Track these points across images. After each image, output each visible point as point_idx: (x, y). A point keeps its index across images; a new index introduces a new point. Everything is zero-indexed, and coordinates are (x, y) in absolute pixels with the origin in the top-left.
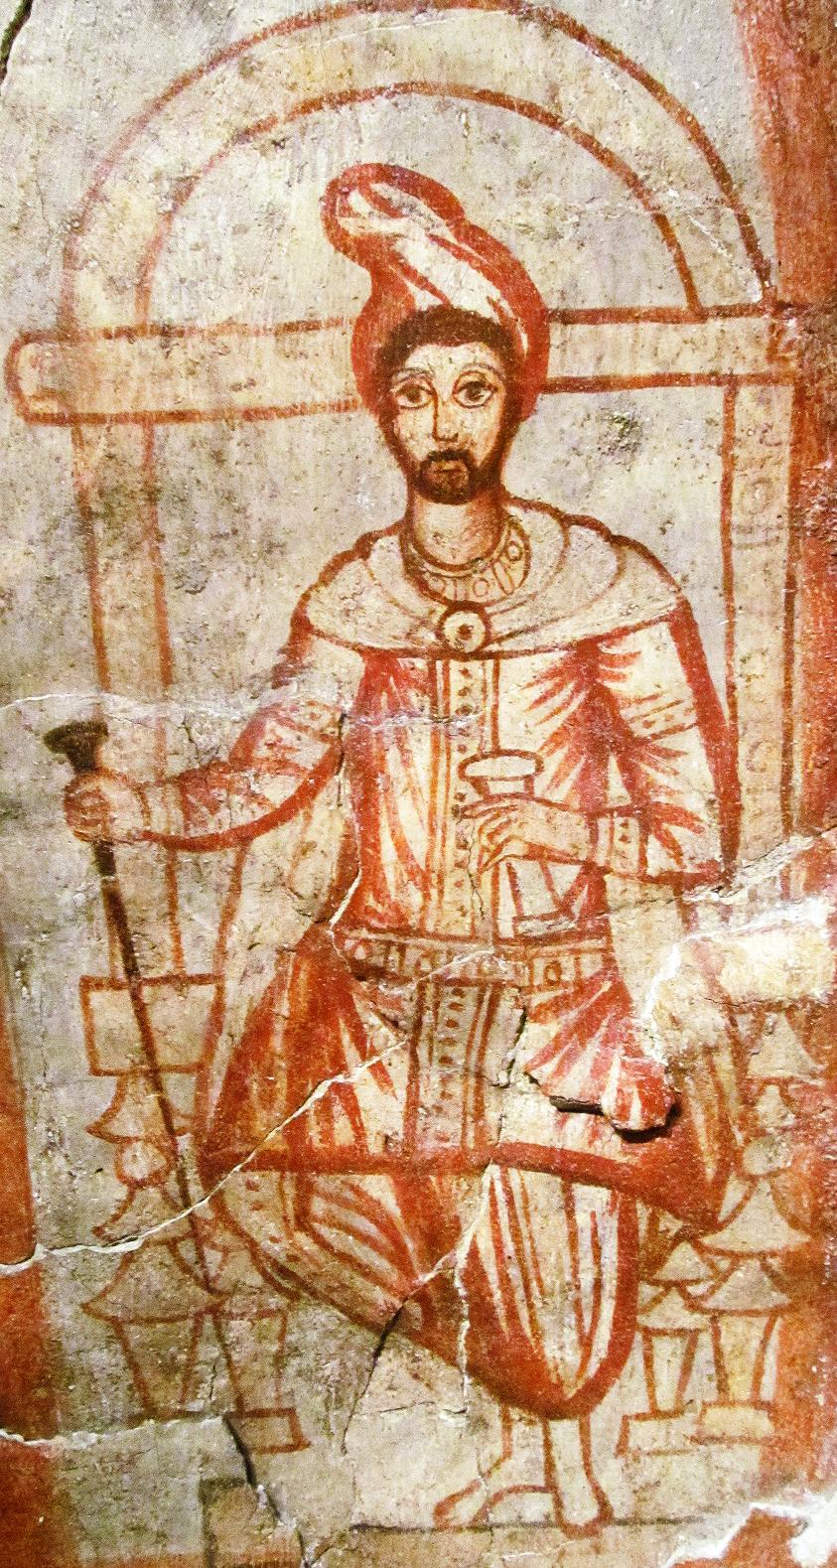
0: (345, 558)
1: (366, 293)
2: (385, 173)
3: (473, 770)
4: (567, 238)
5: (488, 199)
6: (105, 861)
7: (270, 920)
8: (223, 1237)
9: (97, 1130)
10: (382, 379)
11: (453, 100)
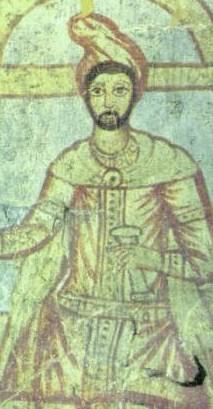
3: (115, 233)
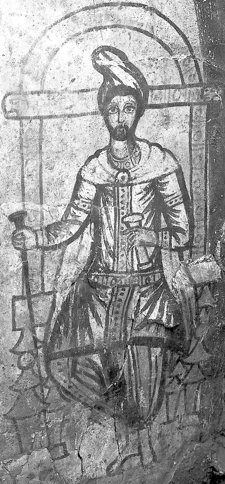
0: (90, 158)
1: (102, 81)
2: (109, 48)
3: (127, 219)
4: (154, 66)
5: (134, 56)
6: (24, 256)
7: (69, 271)
8: (50, 383)
9: (13, 351)
10: (105, 107)
11: (127, 30)
